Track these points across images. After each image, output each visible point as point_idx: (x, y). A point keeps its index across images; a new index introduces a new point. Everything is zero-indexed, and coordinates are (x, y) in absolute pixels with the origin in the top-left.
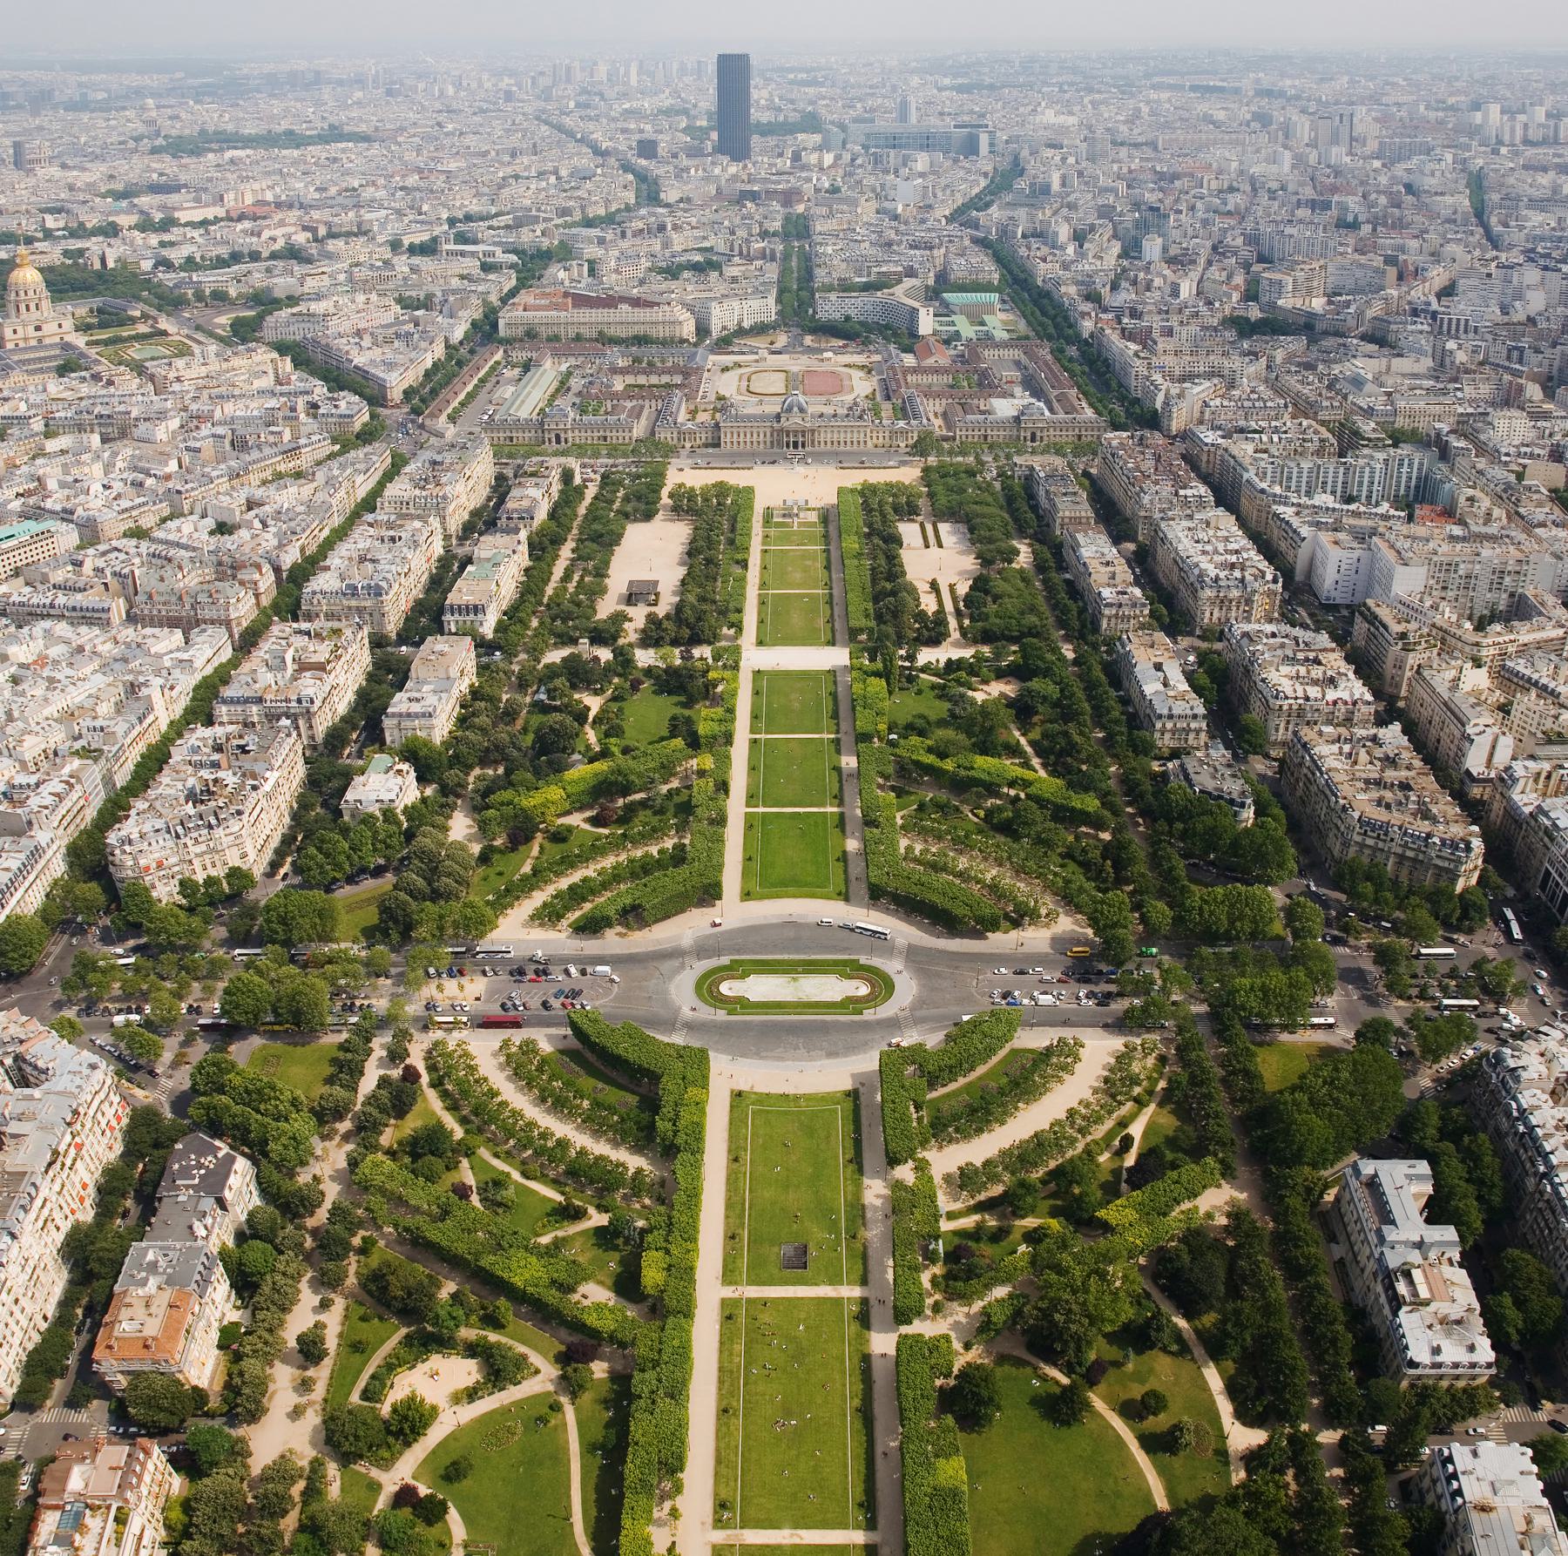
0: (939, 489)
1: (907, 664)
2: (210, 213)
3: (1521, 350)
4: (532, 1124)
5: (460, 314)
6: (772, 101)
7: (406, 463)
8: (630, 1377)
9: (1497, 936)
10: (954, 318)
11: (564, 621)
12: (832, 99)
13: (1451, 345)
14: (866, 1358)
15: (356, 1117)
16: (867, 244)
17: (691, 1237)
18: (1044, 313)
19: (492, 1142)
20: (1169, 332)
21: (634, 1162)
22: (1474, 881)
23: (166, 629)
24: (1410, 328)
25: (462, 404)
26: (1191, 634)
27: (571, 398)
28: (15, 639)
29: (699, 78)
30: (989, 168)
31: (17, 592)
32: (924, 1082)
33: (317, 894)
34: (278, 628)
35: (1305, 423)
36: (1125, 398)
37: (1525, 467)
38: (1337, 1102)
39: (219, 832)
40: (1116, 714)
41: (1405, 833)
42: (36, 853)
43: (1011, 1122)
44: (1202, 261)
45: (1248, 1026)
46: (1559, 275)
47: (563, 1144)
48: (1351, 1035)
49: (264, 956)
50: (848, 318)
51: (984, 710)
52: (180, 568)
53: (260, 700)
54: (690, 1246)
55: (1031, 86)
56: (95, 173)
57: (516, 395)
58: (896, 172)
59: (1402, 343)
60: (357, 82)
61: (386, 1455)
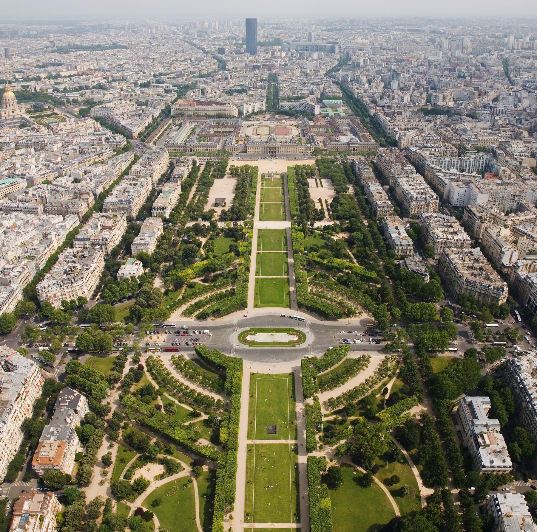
0: (322, 167)
1: (311, 227)
2: (72, 73)
3: (521, 120)
4: (182, 384)
5: (158, 107)
6: (265, 35)
7: (139, 158)
8: (216, 471)
9: (513, 320)
10: (327, 109)
11: (193, 212)
12: (285, 34)
13: (497, 118)
14: (297, 464)
15: (122, 382)
16: (297, 84)
17: (237, 423)
18: (358, 107)
19: (169, 390)
20: (400, 114)
21: (217, 397)
22: (505, 301)
23: (57, 215)
24: (483, 112)
25: (158, 138)
26: (408, 217)
27: (196, 136)
28: (5, 219)
29: (239, 27)
30: (339, 57)
31: (6, 202)
32: (316, 370)
33: (109, 306)
34: (95, 215)
35: (447, 145)
36: (385, 136)
37: (522, 160)
38: (458, 377)
39: (75, 285)
40: (382, 244)
41: (481, 285)
42: (12, 292)
43: (346, 384)
44: (412, 89)
45: (428, 351)
46: (534, 94)
47: (193, 391)
48: (463, 354)
49: (90, 327)
50: (290, 109)
51: (337, 243)
52: (62, 194)
53: (89, 239)
54: (236, 426)
55: (353, 29)
56: (32, 59)
57: (177, 135)
58: (307, 59)
59: (480, 117)
60: (122, 28)
61: (132, 497)
